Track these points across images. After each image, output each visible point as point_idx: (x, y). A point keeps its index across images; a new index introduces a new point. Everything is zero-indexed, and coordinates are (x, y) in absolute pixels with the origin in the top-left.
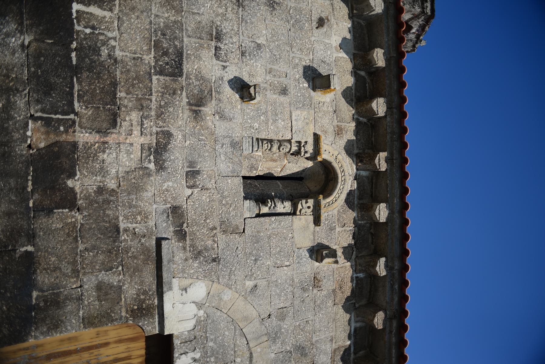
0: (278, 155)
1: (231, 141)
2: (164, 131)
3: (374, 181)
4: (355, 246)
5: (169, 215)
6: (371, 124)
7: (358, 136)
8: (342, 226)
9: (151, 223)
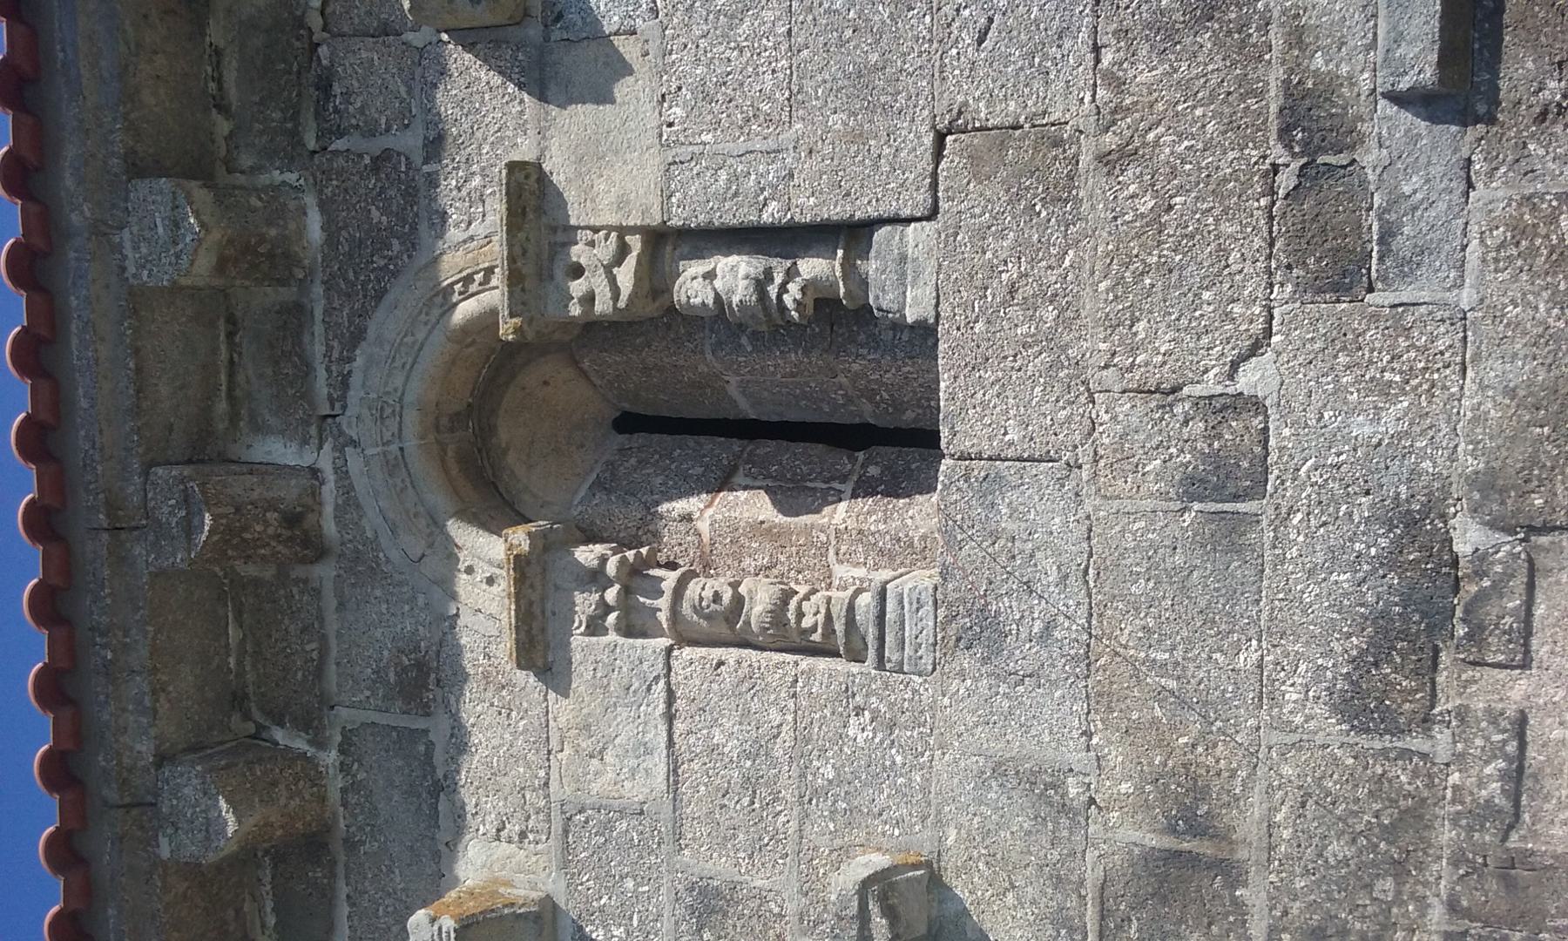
0: (747, 561)
1: (999, 652)
2: (1387, 731)
3: (222, 406)
4: (315, 38)
5: (1382, 241)
6: (247, 716)
7: (315, 655)
8: (389, 159)
9: (1493, 193)
